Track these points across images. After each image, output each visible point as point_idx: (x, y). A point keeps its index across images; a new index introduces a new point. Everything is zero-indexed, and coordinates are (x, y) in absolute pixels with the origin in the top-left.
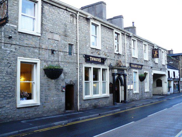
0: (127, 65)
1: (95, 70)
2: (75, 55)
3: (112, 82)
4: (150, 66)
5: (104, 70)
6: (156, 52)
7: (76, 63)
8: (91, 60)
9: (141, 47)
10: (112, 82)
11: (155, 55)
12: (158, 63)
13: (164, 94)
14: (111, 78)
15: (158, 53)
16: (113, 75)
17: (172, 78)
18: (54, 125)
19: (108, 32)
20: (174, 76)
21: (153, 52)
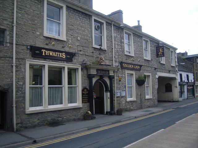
0: (115, 64)
2: (8, 45)
3: (88, 87)
6: (160, 50)
7: (10, 58)
8: (44, 54)
9: (139, 43)
10: (88, 87)
11: (159, 53)
12: (164, 63)
13: (174, 100)
14: (86, 81)
15: (163, 50)
16: (90, 77)
17: (186, 82)
18: (145, 111)
19: (81, 18)
20: (188, 79)
21: (157, 49)
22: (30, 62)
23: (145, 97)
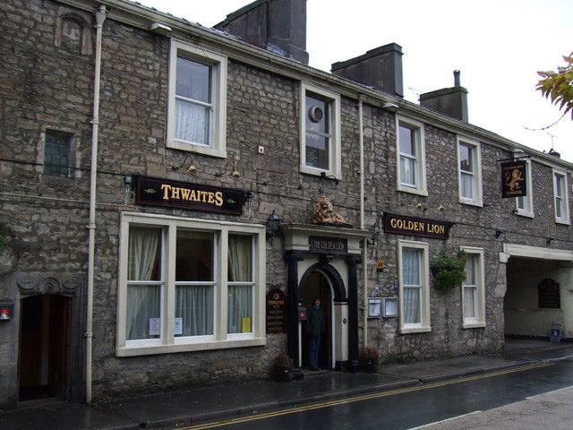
1: (183, 236)
2: (79, 174)
4: (495, 226)
5: (242, 241)
6: (515, 175)
8: (166, 197)
11: (512, 185)
16: (290, 259)
19: (267, 89)
21: (504, 172)
22: (130, 219)
23: (462, 321)
